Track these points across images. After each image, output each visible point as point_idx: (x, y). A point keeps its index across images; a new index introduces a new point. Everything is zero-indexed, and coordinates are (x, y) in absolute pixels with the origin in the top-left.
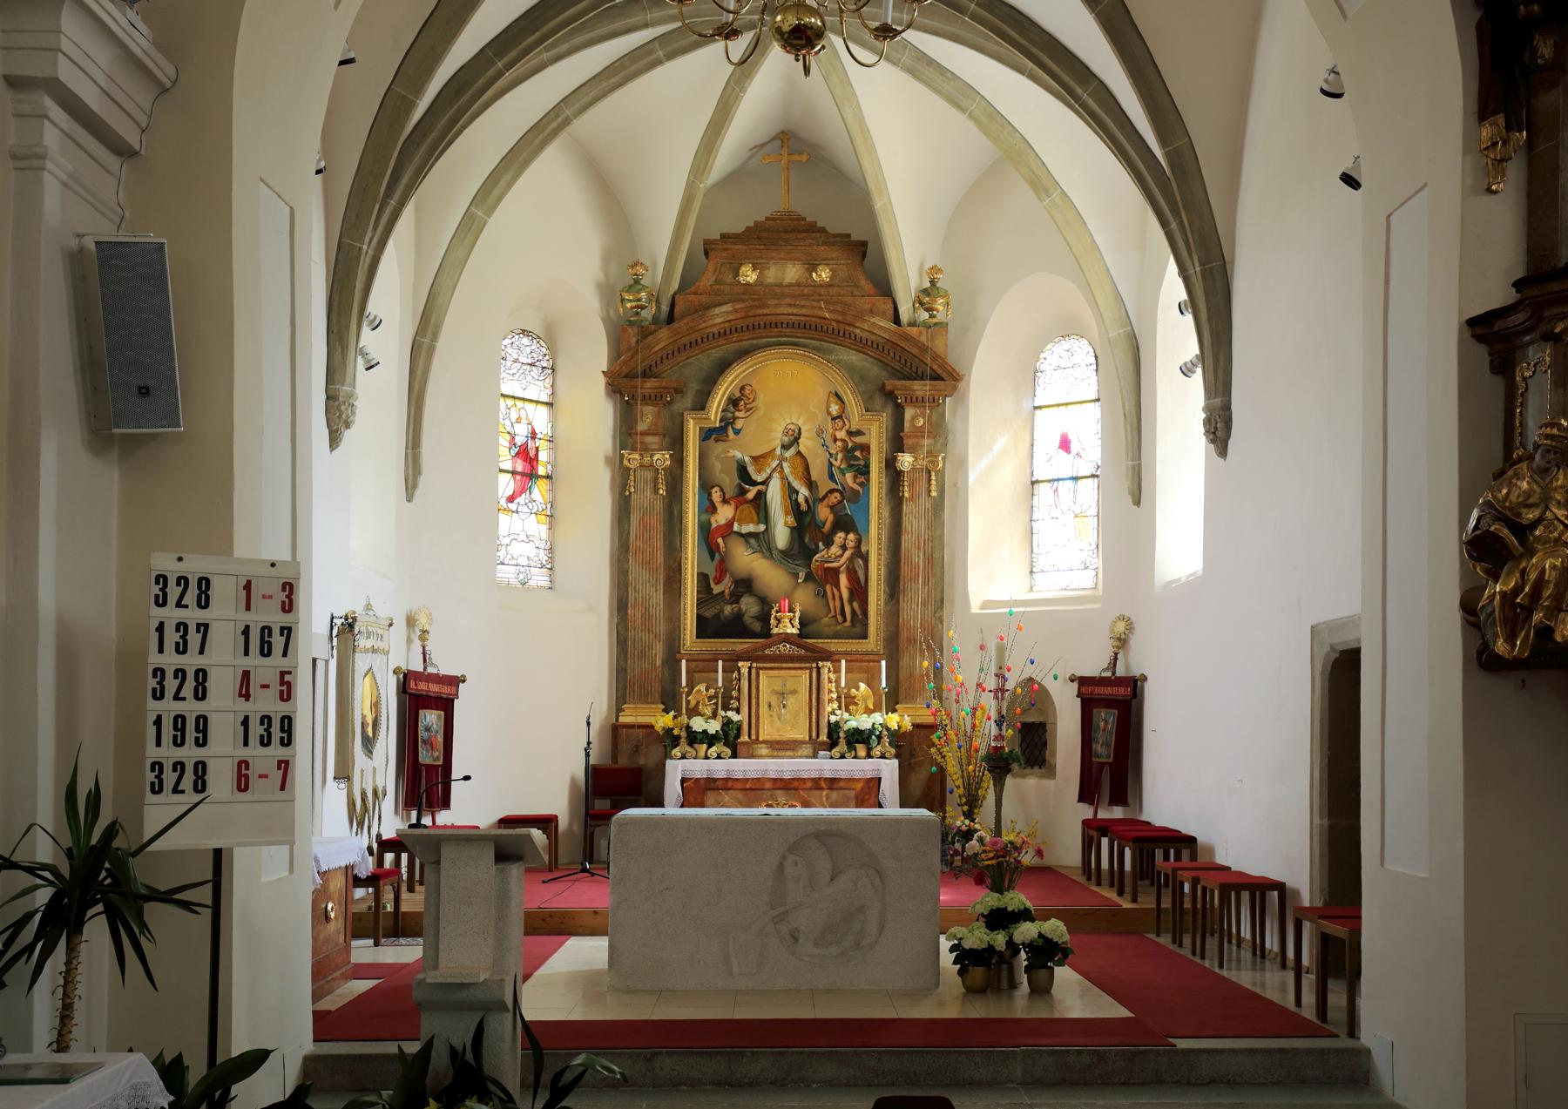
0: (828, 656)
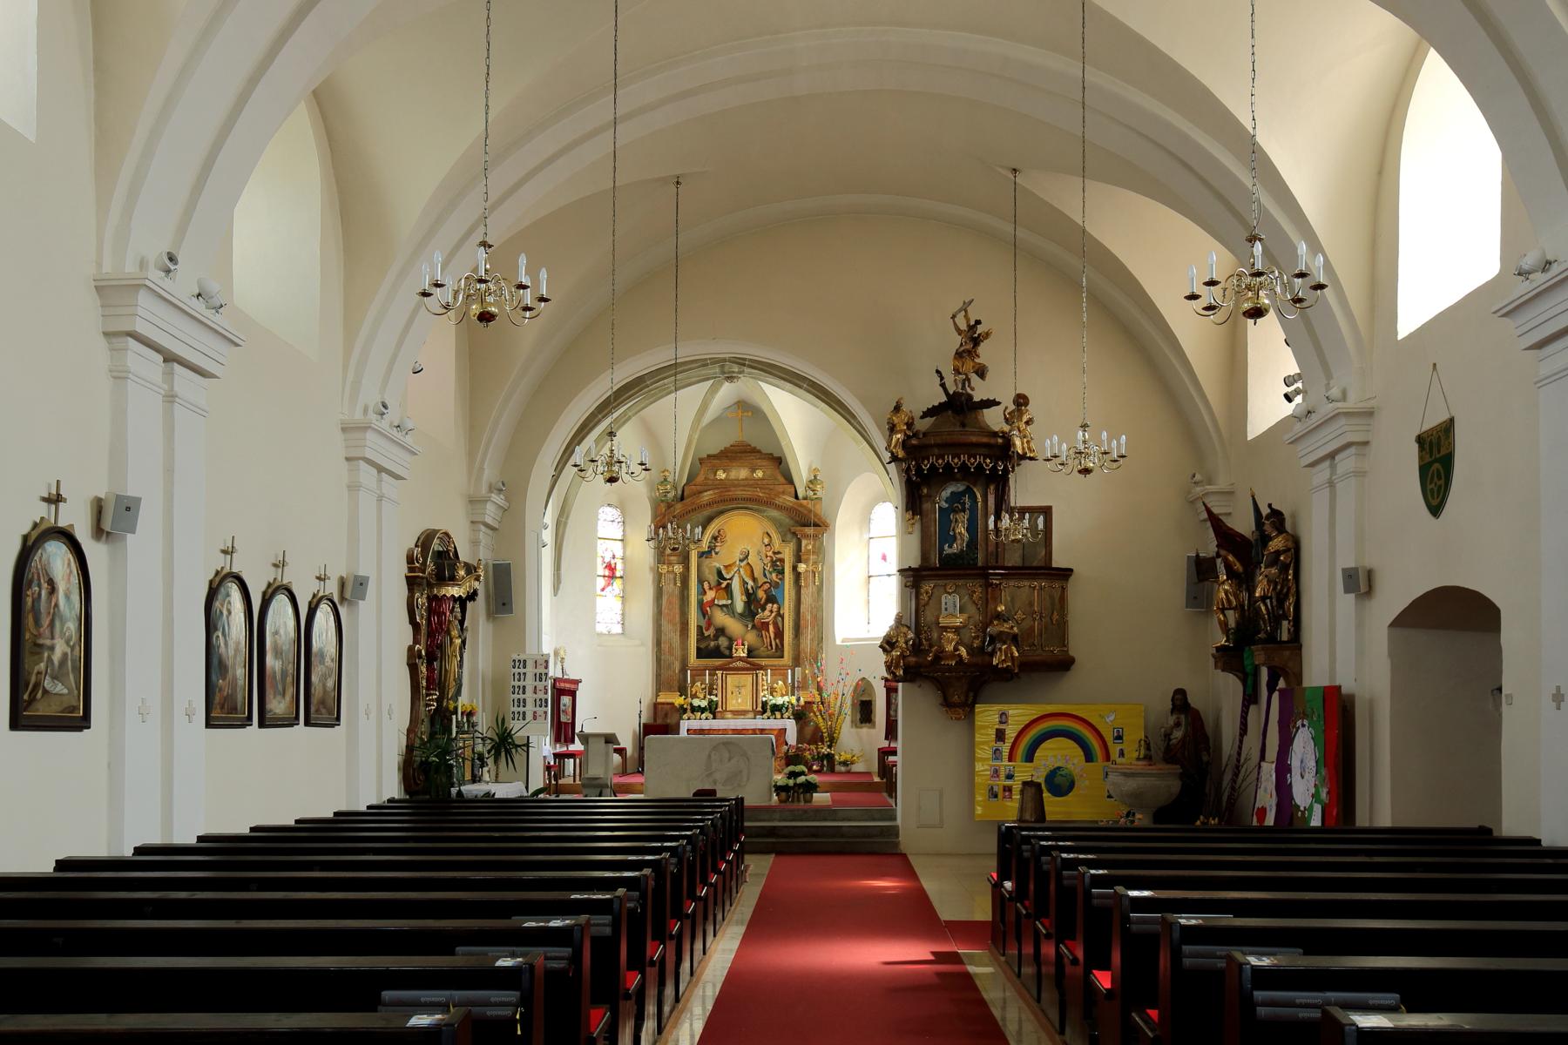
0: (761, 668)
